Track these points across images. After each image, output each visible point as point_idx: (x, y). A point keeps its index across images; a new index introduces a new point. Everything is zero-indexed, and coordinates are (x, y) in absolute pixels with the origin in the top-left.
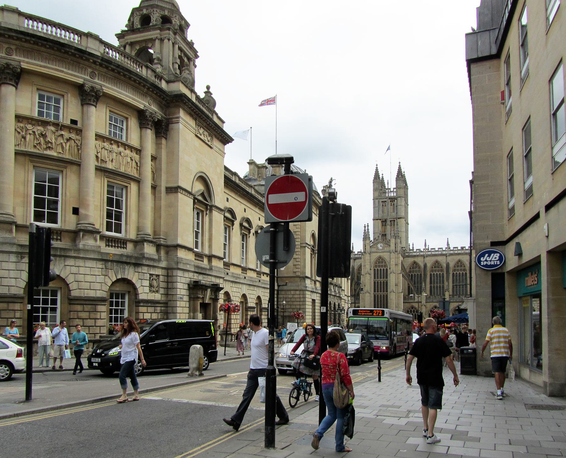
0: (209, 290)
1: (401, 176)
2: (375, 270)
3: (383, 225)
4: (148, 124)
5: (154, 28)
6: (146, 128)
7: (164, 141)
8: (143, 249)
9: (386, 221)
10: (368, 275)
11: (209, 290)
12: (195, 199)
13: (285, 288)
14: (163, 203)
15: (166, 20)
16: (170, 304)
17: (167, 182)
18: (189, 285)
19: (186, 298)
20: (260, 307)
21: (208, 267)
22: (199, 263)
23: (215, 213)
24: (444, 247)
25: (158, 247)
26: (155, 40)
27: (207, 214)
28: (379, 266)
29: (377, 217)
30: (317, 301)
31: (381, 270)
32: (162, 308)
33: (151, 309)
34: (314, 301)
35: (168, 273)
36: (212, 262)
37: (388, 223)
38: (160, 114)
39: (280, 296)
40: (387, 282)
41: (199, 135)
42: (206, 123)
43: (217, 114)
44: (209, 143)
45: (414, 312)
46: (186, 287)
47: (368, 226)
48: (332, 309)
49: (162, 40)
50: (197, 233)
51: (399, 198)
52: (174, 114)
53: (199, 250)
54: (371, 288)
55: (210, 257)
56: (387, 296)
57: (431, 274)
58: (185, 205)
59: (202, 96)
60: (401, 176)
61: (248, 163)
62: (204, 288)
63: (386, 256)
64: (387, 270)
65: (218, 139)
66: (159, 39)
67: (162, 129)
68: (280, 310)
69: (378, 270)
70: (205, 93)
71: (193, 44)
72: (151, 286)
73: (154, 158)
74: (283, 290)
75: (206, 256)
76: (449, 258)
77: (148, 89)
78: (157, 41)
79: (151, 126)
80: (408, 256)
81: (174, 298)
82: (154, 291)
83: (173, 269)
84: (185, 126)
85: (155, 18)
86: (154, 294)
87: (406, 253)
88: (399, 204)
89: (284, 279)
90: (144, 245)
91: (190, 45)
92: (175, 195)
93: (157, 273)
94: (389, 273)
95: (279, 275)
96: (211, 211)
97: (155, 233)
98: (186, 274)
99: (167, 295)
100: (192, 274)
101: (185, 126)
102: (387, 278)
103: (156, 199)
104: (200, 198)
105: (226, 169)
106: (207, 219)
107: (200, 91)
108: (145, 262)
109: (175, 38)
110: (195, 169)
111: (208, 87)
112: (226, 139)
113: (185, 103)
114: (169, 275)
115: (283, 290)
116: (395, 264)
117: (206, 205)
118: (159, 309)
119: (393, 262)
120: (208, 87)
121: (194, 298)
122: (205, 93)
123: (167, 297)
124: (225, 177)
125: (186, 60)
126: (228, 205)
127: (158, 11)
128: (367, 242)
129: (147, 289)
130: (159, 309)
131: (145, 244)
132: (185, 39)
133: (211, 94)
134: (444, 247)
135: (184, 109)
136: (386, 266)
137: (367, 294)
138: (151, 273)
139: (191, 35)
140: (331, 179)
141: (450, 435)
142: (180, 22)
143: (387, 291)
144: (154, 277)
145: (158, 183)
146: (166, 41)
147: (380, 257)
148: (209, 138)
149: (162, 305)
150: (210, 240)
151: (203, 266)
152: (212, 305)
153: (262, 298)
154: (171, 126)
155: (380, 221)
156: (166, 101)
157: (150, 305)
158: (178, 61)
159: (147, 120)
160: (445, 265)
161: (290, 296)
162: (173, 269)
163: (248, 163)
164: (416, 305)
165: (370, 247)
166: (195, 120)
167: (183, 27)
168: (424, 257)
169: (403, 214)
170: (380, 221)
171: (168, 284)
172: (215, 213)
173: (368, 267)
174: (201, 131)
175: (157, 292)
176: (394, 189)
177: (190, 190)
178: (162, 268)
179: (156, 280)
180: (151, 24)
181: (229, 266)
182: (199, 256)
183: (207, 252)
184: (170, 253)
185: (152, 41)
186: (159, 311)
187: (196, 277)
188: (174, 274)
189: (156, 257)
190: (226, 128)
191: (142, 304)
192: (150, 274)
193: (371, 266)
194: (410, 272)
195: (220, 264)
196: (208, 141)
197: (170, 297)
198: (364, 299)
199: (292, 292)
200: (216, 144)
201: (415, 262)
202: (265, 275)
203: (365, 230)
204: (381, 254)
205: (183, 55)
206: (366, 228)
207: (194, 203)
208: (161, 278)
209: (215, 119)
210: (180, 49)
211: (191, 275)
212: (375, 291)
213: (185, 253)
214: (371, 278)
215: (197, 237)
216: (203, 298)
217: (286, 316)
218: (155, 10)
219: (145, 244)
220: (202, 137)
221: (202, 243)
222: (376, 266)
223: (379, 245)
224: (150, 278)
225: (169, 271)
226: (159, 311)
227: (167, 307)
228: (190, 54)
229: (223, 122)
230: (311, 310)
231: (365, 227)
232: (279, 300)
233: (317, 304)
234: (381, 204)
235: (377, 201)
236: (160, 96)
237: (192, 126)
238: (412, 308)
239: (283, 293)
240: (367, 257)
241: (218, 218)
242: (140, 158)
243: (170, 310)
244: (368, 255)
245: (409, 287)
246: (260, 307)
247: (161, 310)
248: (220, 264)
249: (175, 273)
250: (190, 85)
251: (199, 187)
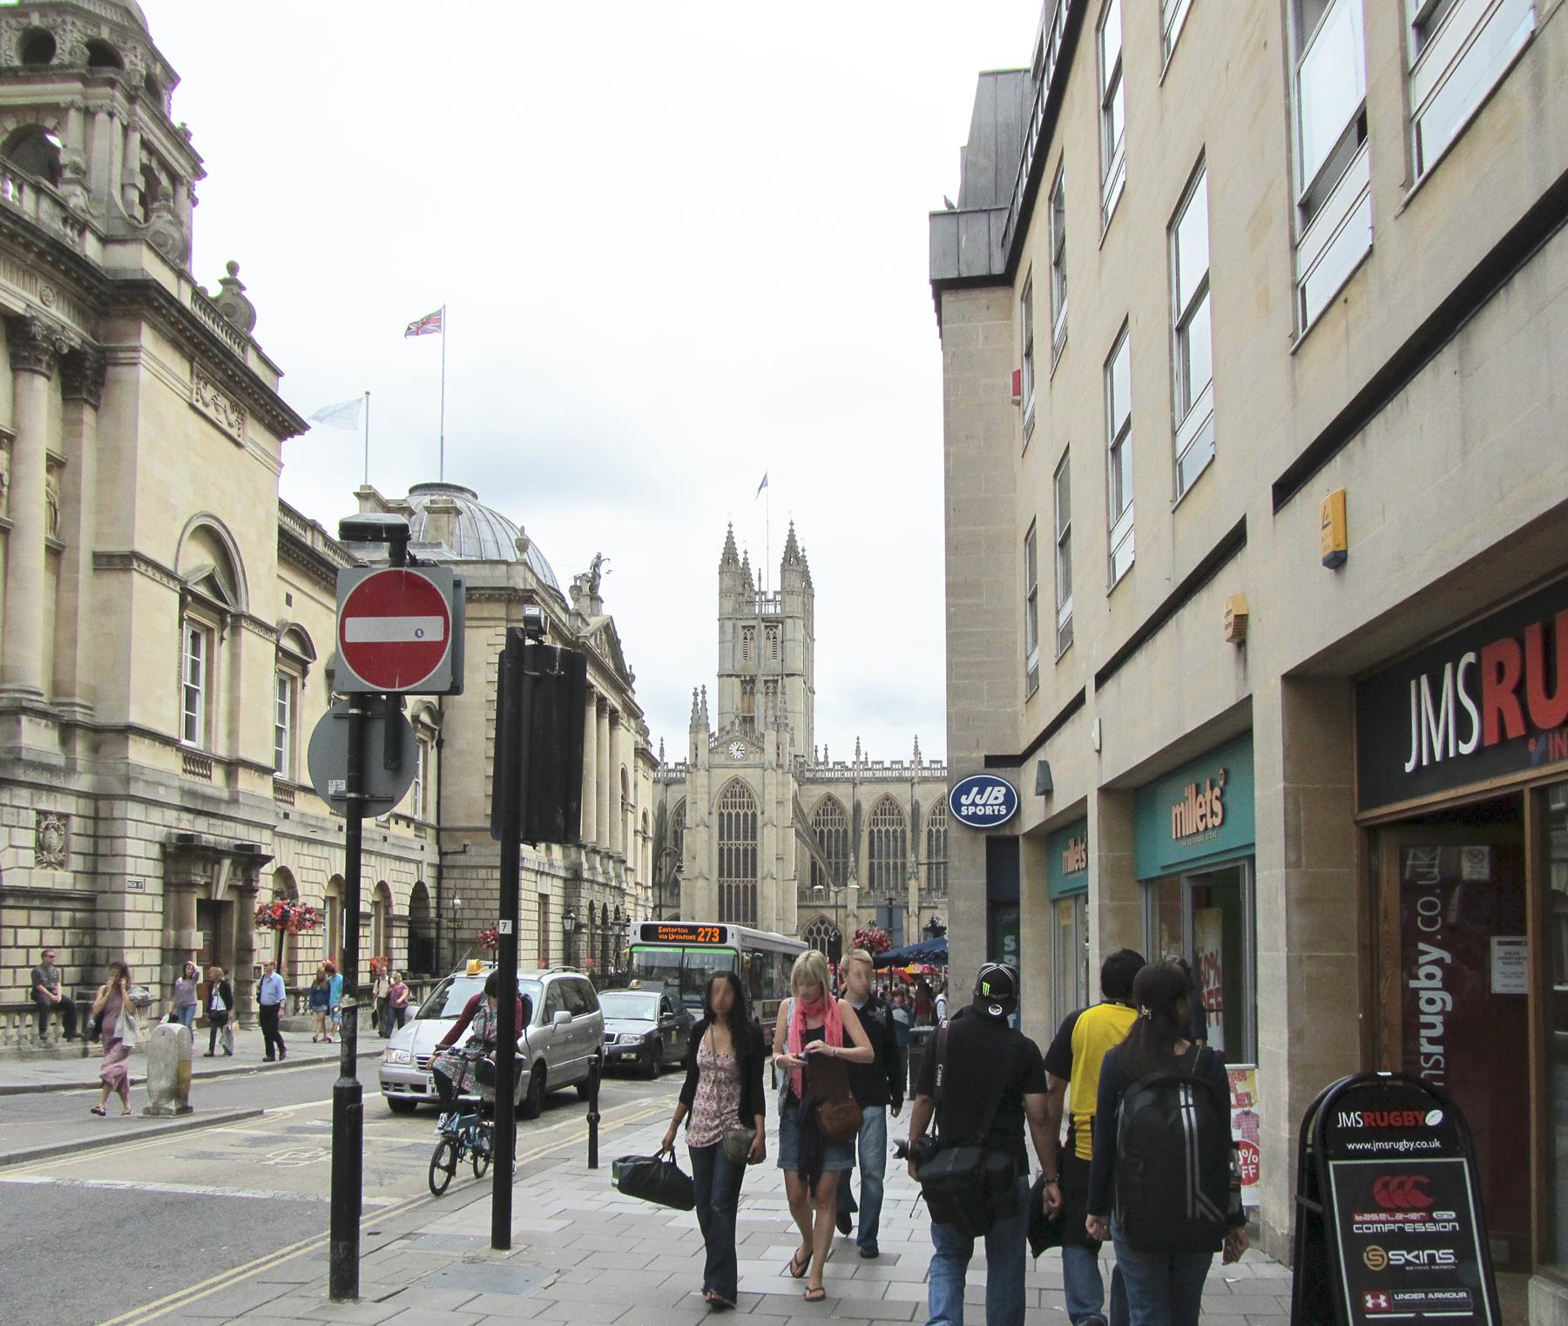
0: (227, 863)
1: (793, 559)
2: (721, 815)
3: (744, 693)
4: (40, 361)
5: (64, 73)
6: (34, 372)
7: (88, 415)
8: (16, 734)
9: (753, 681)
10: (701, 828)
11: (227, 863)
12: (185, 593)
13: (461, 860)
14: (84, 598)
15: (102, 56)
16: (102, 901)
17: (98, 537)
18: (163, 845)
19: (155, 886)
20: (387, 913)
21: (225, 795)
22: (199, 784)
23: (248, 637)
24: (907, 758)
25: (67, 730)
26: (66, 110)
27: (222, 639)
28: (734, 805)
29: (729, 669)
30: (552, 900)
31: (738, 815)
32: (78, 915)
33: (40, 918)
34: (544, 898)
35: (97, 810)
36: (236, 780)
37: (760, 686)
38: (79, 335)
39: (445, 883)
40: (754, 850)
41: (200, 405)
42: (224, 371)
43: (257, 349)
44: (233, 432)
45: (826, 931)
46: (155, 851)
47: (704, 692)
48: (598, 922)
49: (88, 114)
50: (191, 695)
51: (789, 621)
52: (121, 338)
53: (197, 744)
54: (710, 864)
55: (232, 767)
56: (754, 887)
57: (872, 832)
58: (154, 612)
59: (215, 291)
60: (793, 559)
61: (358, 495)
62: (211, 856)
63: (751, 777)
64: (754, 815)
65: (260, 420)
66: (78, 109)
67: (85, 378)
68: (444, 923)
69: (730, 815)
70: (224, 282)
71: (188, 134)
72: (41, 846)
73: (55, 464)
74: (454, 867)
75: (219, 761)
76: (920, 790)
77: (41, 255)
78: (73, 114)
79: (48, 365)
80: (813, 781)
81: (117, 884)
82: (50, 864)
83: (111, 797)
84: (156, 374)
85: (70, 42)
86: (50, 871)
87: (806, 772)
88: (789, 635)
89: (460, 834)
90: (19, 722)
91: (181, 138)
92: (122, 576)
93: (60, 809)
94: (759, 824)
95: (443, 824)
96: (235, 630)
97: (56, 688)
98: (156, 815)
99: (93, 873)
100: (174, 813)
101: (156, 374)
102: (754, 838)
103: (63, 587)
104: (202, 590)
105: (285, 508)
106: (222, 653)
107: (208, 274)
108: (22, 775)
109: (132, 113)
110: (188, 506)
111: (233, 268)
112: (284, 424)
113: (157, 309)
114: (102, 815)
115: (454, 867)
116: (776, 800)
117: (222, 613)
118: (65, 918)
119: (771, 795)
120: (233, 268)
121: (177, 885)
122: (224, 282)
123: (94, 881)
124: (283, 533)
125: (164, 180)
126: (291, 616)
127: (79, 24)
128: (703, 736)
129: (28, 857)
130: (65, 918)
131: (24, 719)
132: (162, 120)
133: (242, 288)
134: (907, 758)
135: (154, 327)
136: (751, 805)
137: (701, 883)
138: (43, 806)
139: (181, 108)
140: (599, 557)
141: (57, 450)
142: (148, 67)
143: (754, 875)
144: (53, 820)
145: (67, 540)
146: (102, 117)
147: (737, 781)
148: (233, 417)
149: (77, 905)
150: (233, 715)
151: (210, 791)
152: (236, 905)
153: (393, 888)
154: (112, 372)
155: (737, 681)
156: (97, 296)
157: (36, 903)
158: (140, 181)
159: (36, 348)
160: (908, 808)
161: (476, 884)
162: (111, 797)
163: (358, 495)
164: (830, 914)
165: (710, 751)
166: (191, 360)
167: (156, 85)
168: (855, 785)
169: (798, 666)
170: (737, 681)
171: (96, 844)
172: (248, 637)
173: (703, 806)
174: (209, 393)
175: (61, 864)
176: (776, 593)
177: (170, 566)
178: (80, 794)
179: (57, 829)
180: (55, 61)
181: (292, 794)
182: (197, 761)
183: (221, 750)
184: (103, 750)
185: (59, 111)
186: (66, 923)
187: (188, 824)
188: (117, 814)
189: (59, 760)
190: (287, 391)
191: (10, 902)
192: (39, 812)
193: (711, 805)
194: (817, 823)
195: (265, 788)
196: (230, 425)
197: (102, 883)
198: (691, 897)
199: (483, 873)
200: (255, 434)
201: (830, 798)
202: (402, 823)
203: (695, 704)
204: (741, 773)
205: (154, 165)
206: (700, 698)
207: (183, 605)
208: (76, 825)
209: (253, 363)
210: (146, 145)
211: (171, 816)
212: (721, 874)
213: (151, 751)
214: (710, 836)
215: (279, 742)
216: (207, 886)
217: (464, 942)
218: (69, 19)
219: (24, 719)
220: (211, 412)
221: (208, 723)
222: (725, 805)
223: (733, 748)
224: (38, 823)
225: (101, 803)
226: (66, 923)
227: (93, 911)
228: (180, 164)
229: (278, 373)
230: (535, 926)
231: (696, 694)
232: (444, 894)
233: (552, 908)
234: (741, 633)
235: (729, 624)
236: (78, 281)
237: (178, 379)
238: (823, 922)
239: (456, 873)
240: (701, 777)
241: (258, 652)
242: (11, 460)
243: (102, 920)
244: (702, 773)
245: (814, 865)
246: (387, 913)
247: (73, 919)
248: (265, 788)
249: (119, 809)
250: (178, 256)
251: (199, 559)
